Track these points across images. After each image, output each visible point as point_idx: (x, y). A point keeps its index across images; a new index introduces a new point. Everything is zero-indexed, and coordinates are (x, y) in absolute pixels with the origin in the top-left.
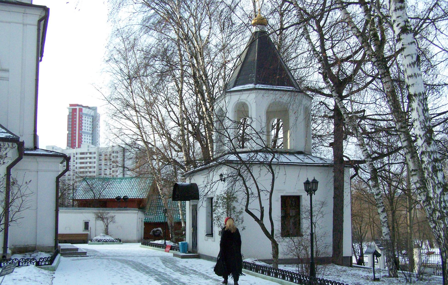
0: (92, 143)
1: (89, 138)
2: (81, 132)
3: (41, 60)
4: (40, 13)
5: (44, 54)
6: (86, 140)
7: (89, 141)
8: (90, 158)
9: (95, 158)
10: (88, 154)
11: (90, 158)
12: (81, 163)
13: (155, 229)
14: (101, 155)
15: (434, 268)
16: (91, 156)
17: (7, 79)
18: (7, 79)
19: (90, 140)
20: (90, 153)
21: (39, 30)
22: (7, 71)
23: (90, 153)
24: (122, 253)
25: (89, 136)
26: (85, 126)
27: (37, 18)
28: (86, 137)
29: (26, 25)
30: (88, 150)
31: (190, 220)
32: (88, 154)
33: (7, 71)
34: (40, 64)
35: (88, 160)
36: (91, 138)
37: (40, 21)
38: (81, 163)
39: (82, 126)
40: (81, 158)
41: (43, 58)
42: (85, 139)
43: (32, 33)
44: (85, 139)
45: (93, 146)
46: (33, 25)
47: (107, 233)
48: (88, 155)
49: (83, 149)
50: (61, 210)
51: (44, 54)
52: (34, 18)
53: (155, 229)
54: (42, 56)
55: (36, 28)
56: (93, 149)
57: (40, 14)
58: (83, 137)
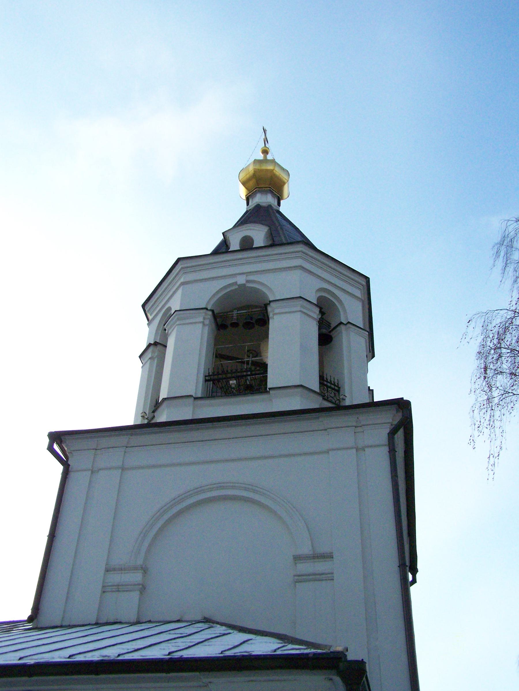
3: (414, 581)
4: (390, 418)
5: (419, 566)
15: (296, 564)
17: (327, 577)
18: (327, 577)
21: (392, 451)
22: (328, 556)
27: (385, 431)
29: (363, 449)
31: (207, 355)
33: (328, 556)
34: (413, 589)
37: (392, 433)
41: (418, 575)
43: (378, 462)
46: (378, 446)
50: (343, 404)
51: (420, 565)
52: (377, 431)
54: (414, 570)
55: (385, 450)
57: (391, 421)
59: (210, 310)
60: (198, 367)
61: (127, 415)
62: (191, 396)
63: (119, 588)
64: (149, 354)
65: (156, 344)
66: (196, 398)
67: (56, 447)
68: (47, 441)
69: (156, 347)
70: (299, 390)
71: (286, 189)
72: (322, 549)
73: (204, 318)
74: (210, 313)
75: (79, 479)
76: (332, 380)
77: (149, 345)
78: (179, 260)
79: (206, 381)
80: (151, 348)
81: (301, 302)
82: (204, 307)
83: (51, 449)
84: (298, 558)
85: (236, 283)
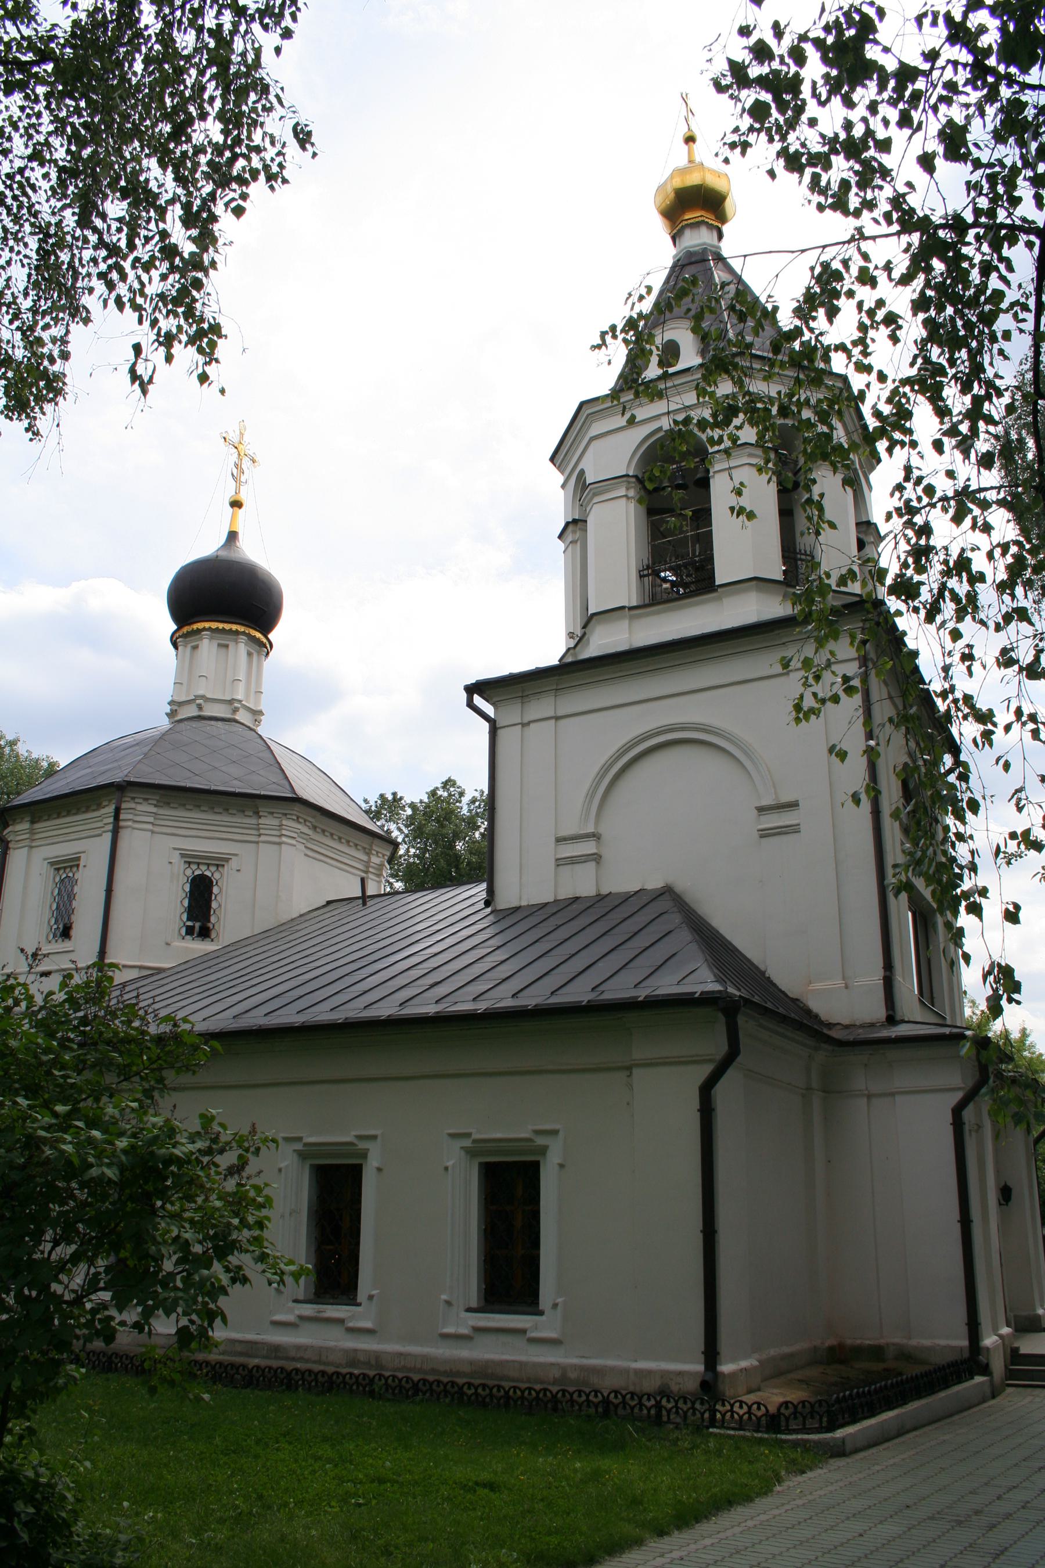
17: (792, 830)
18: (792, 830)
22: (793, 805)
59: (632, 476)
60: (416, 1387)
61: (548, 649)
62: (623, 608)
63: (573, 861)
64: (570, 537)
65: (575, 522)
66: (631, 608)
67: (478, 700)
68: (464, 695)
69: (575, 527)
70: (754, 583)
71: (728, 204)
72: (785, 798)
73: (627, 489)
74: (634, 480)
75: (508, 738)
76: (802, 548)
77: (567, 524)
78: (582, 405)
79: (641, 577)
80: (571, 528)
81: (747, 450)
82: (624, 473)
83: (471, 705)
84: (761, 810)
85: (660, 429)
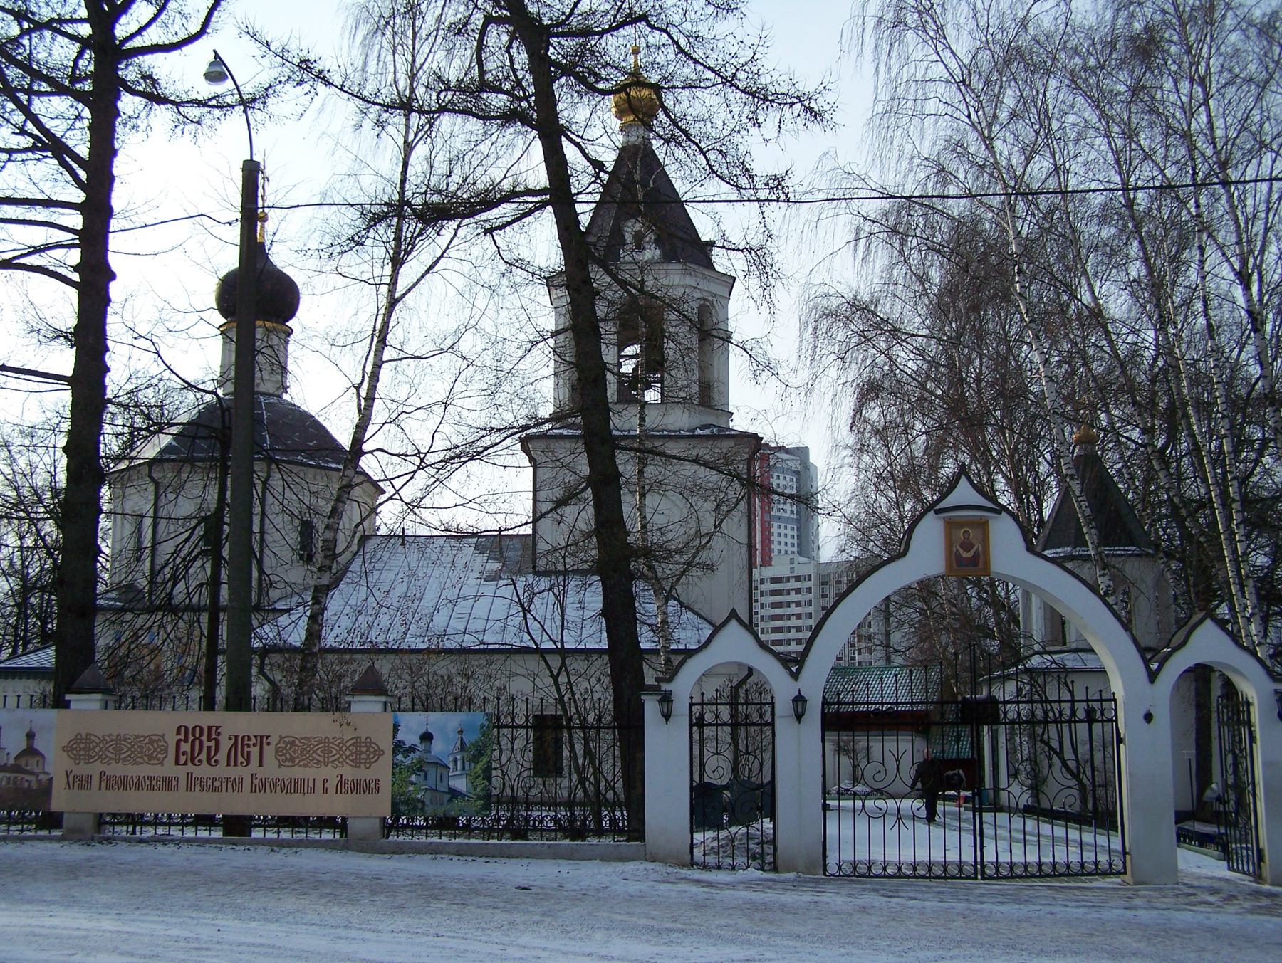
0: (800, 553)
1: (789, 532)
2: (767, 518)
6: (782, 547)
7: (789, 541)
8: (798, 591)
9: (809, 590)
10: (792, 581)
11: (798, 591)
12: (774, 605)
13: (950, 773)
14: (825, 583)
16: (799, 585)
19: (793, 537)
20: (798, 579)
23: (798, 579)
24: (197, 907)
25: (788, 477)
26: (779, 543)
28: (782, 531)
30: (792, 570)
32: (792, 581)
35: (793, 597)
36: (795, 533)
38: (774, 605)
39: (771, 542)
40: (774, 593)
42: (779, 535)
44: (779, 535)
45: (802, 560)
47: (855, 780)
48: (793, 584)
49: (779, 567)
53: (950, 773)
56: (804, 567)
58: (775, 530)
